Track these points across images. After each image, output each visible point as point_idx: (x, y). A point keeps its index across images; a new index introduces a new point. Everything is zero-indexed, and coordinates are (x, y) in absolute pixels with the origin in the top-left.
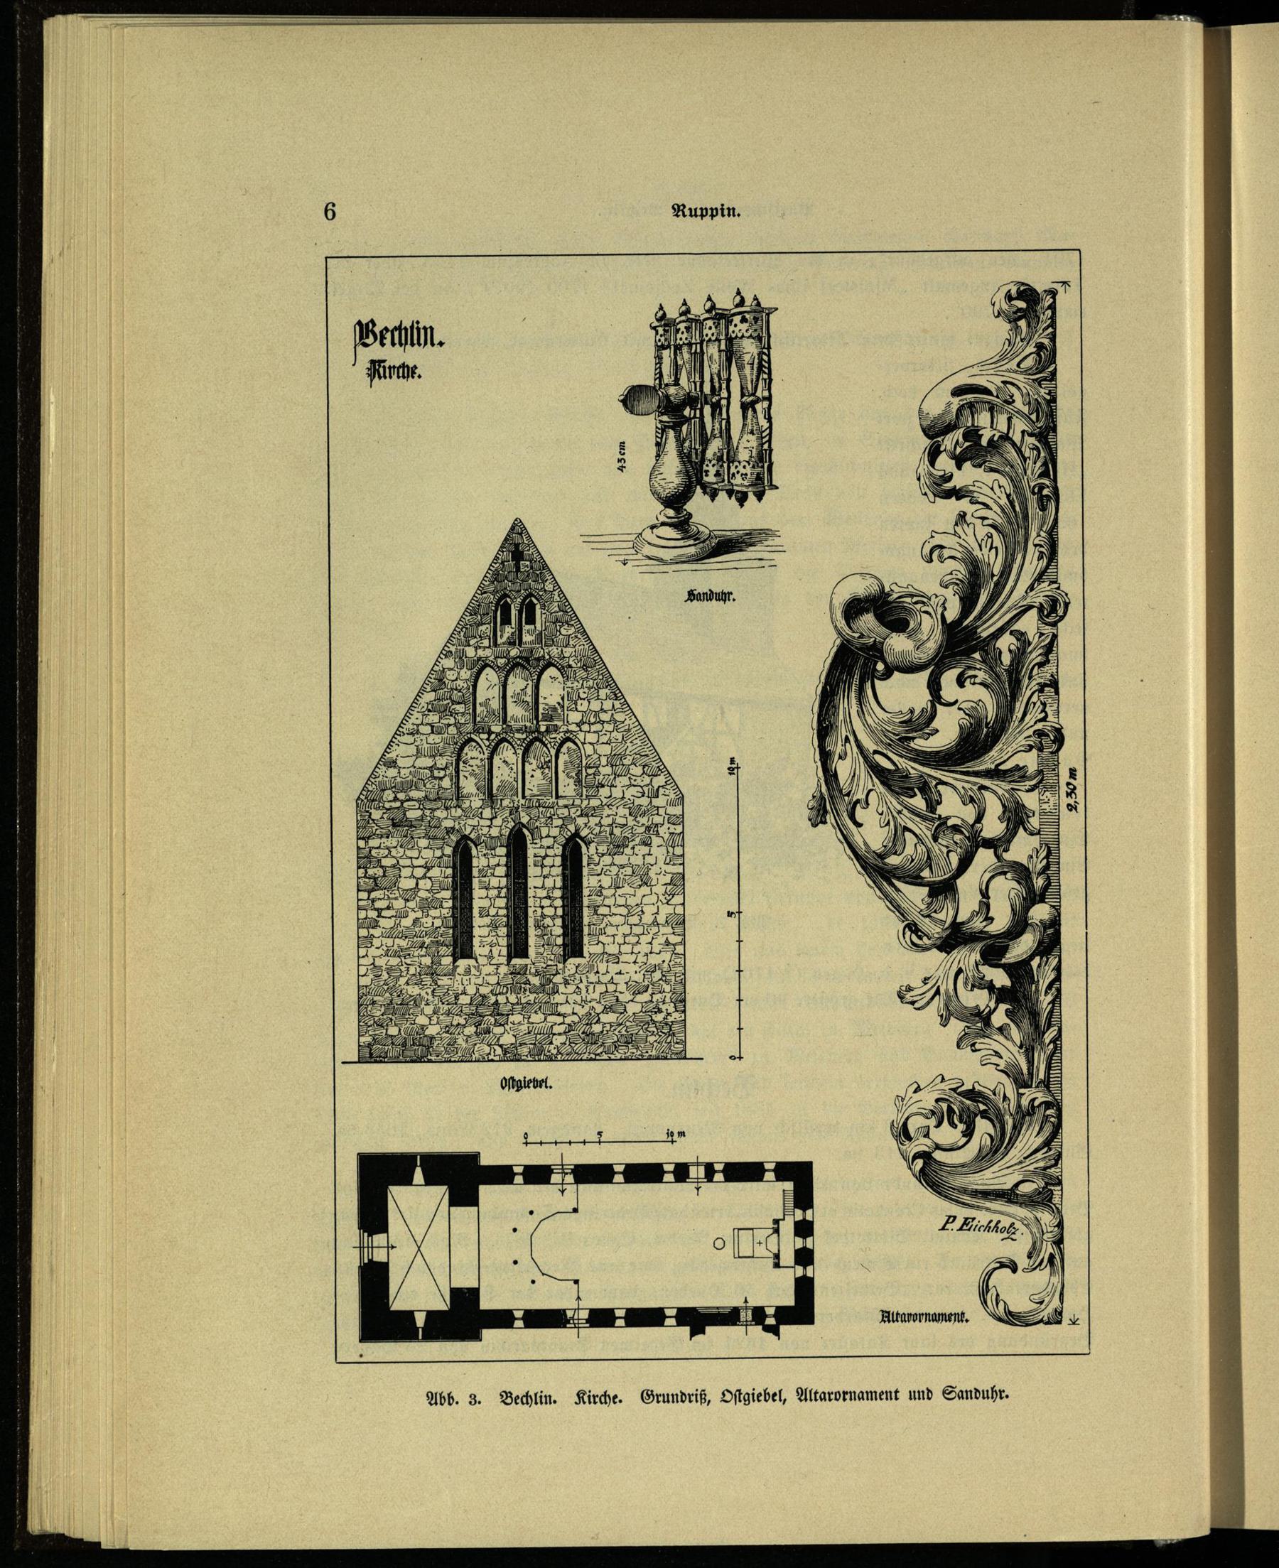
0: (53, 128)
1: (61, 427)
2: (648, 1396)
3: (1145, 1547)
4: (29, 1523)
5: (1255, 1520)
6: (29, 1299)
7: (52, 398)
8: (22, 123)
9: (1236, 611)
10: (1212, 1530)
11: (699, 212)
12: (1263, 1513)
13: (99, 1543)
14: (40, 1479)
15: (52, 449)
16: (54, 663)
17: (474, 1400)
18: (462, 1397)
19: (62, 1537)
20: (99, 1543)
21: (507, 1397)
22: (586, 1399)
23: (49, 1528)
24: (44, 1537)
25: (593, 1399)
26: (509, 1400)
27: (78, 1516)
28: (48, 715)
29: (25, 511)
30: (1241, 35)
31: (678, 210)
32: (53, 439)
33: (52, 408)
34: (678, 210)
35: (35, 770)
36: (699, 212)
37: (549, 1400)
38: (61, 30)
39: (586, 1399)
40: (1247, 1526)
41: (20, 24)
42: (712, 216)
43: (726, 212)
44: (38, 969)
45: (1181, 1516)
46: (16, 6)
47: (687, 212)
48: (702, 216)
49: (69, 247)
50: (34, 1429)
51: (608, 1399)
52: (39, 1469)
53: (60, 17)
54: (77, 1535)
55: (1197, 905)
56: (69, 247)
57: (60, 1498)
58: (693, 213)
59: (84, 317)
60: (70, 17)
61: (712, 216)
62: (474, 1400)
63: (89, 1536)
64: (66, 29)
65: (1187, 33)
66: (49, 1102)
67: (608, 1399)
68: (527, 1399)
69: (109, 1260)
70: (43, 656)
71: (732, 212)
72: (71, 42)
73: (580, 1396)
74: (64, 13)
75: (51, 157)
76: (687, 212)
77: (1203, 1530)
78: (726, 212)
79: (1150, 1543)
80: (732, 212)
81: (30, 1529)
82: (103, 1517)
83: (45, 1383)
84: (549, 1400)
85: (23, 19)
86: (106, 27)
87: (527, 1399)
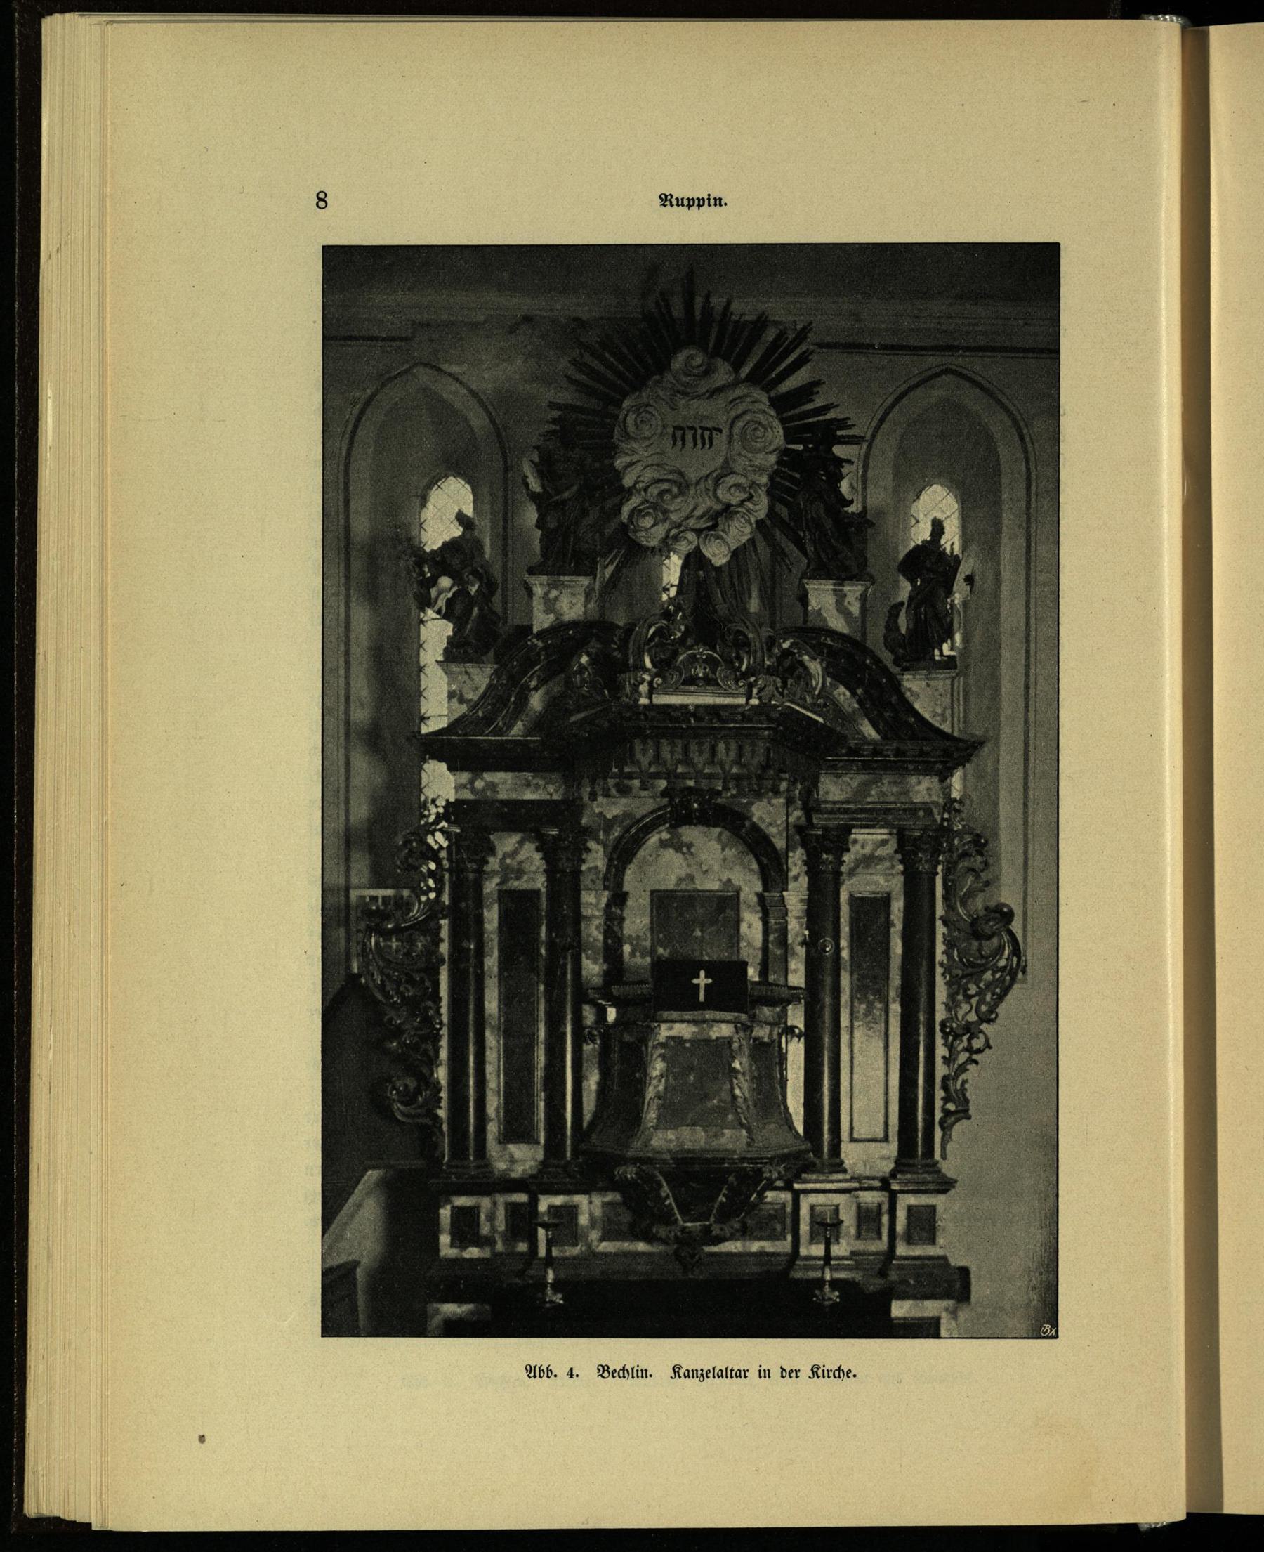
4: (26, 1506)
5: (1236, 1502)
6: (26, 1284)
7: (50, 393)
8: (20, 120)
9: (1214, 560)
10: (1188, 1514)
11: (686, 202)
13: (90, 1524)
14: (36, 1463)
15: (50, 443)
16: (51, 655)
18: (562, 1371)
19: (58, 1521)
20: (90, 1524)
22: (820, 1373)
23: (45, 1511)
24: (40, 1520)
25: (828, 1374)
26: (606, 1374)
27: (72, 1499)
28: (45, 706)
29: (23, 505)
30: (1218, 34)
31: (665, 199)
32: (50, 433)
33: (50, 402)
34: (665, 199)
35: (32, 761)
36: (686, 202)
37: (644, 1374)
38: (59, 29)
39: (820, 1373)
40: (1229, 1509)
41: (19, 22)
42: (699, 206)
43: (712, 202)
44: (36, 958)
46: (15, 5)
47: (674, 202)
48: (689, 206)
50: (30, 1413)
52: (36, 1452)
53: (58, 17)
55: (1175, 1046)
56: (66, 244)
57: (60, 1482)
58: (680, 203)
59: (80, 311)
60: (68, 16)
61: (699, 206)
64: (64, 27)
65: (1163, 34)
66: (46, 1090)
71: (718, 202)
72: (68, 40)
73: (676, 1371)
74: (62, 11)
76: (674, 202)
77: (1180, 1516)
78: (712, 202)
80: (718, 202)
82: (93, 1501)
83: (42, 1367)
84: (644, 1374)
85: (21, 16)
86: (99, 24)
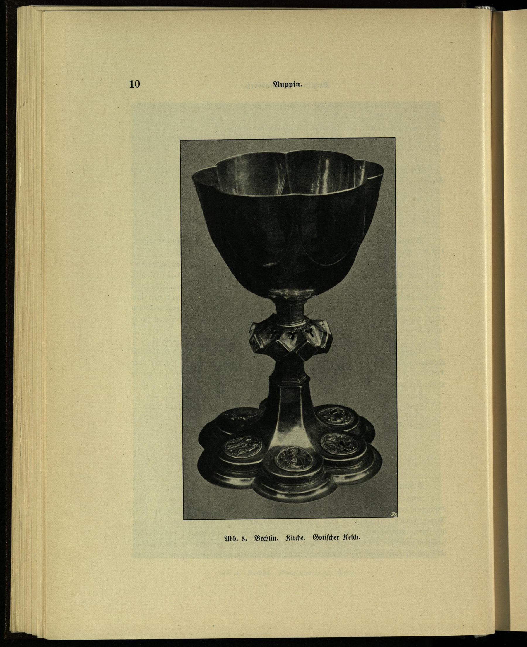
0: (21, 53)
1: (24, 176)
2: (316, 537)
3: (470, 638)
4: (10, 628)
5: (515, 627)
6: (11, 536)
7: (20, 164)
10: (496, 631)
11: (285, 85)
12: (518, 624)
14: (15, 610)
15: (20, 185)
16: (21, 273)
17: (243, 539)
19: (24, 634)
21: (257, 538)
23: (19, 630)
24: (17, 634)
25: (294, 538)
26: (258, 539)
28: (18, 295)
29: (9, 211)
31: (276, 84)
32: (20, 181)
33: (20, 168)
34: (276, 84)
35: (13, 317)
36: (285, 85)
37: (275, 539)
43: (296, 85)
44: (14, 400)
45: (484, 626)
47: (280, 85)
48: (286, 87)
49: (27, 102)
51: (299, 538)
53: (23, 7)
54: (29, 632)
56: (27, 102)
57: (23, 618)
58: (282, 85)
60: (28, 7)
61: (290, 86)
62: (243, 539)
63: (34, 634)
66: (19, 454)
67: (299, 538)
68: (266, 538)
69: (41, 520)
70: (16, 271)
71: (298, 85)
73: (288, 537)
74: (26, 5)
75: (20, 64)
76: (280, 85)
77: (492, 631)
78: (296, 85)
79: (472, 637)
80: (298, 85)
81: (11, 630)
82: (38, 625)
83: (17, 570)
84: (275, 539)
85: (9, 7)
87: (266, 538)
